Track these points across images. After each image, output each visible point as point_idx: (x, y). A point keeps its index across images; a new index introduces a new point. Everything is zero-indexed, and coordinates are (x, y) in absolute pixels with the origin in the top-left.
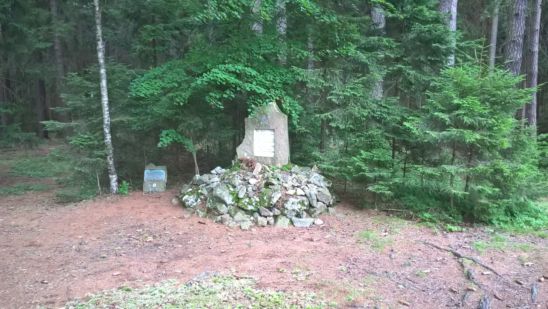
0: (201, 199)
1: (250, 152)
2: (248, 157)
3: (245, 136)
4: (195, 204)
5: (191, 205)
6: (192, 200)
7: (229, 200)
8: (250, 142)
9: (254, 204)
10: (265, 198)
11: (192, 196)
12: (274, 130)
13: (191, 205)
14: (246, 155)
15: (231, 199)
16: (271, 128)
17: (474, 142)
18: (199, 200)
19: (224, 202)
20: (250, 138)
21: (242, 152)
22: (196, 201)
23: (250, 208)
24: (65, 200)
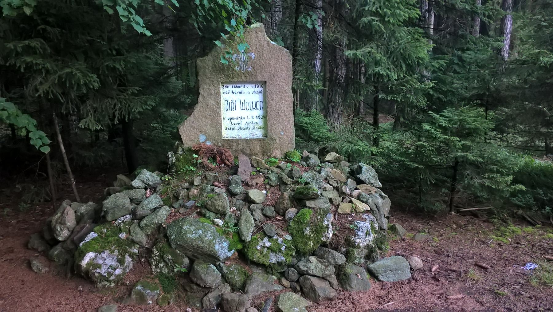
0: (132, 255)
1: (210, 131)
2: (208, 143)
3: (200, 98)
4: (118, 272)
5: (110, 274)
6: (109, 262)
7: (223, 249)
8: (213, 111)
9: (283, 248)
10: (307, 231)
11: (107, 252)
12: (264, 84)
13: (110, 274)
14: (202, 138)
15: (225, 245)
16: (260, 79)
17: (134, 177)
18: (128, 259)
19: (212, 258)
20: (212, 102)
21: (192, 132)
22: (121, 261)
23: (274, 259)
24: (294, 90)
